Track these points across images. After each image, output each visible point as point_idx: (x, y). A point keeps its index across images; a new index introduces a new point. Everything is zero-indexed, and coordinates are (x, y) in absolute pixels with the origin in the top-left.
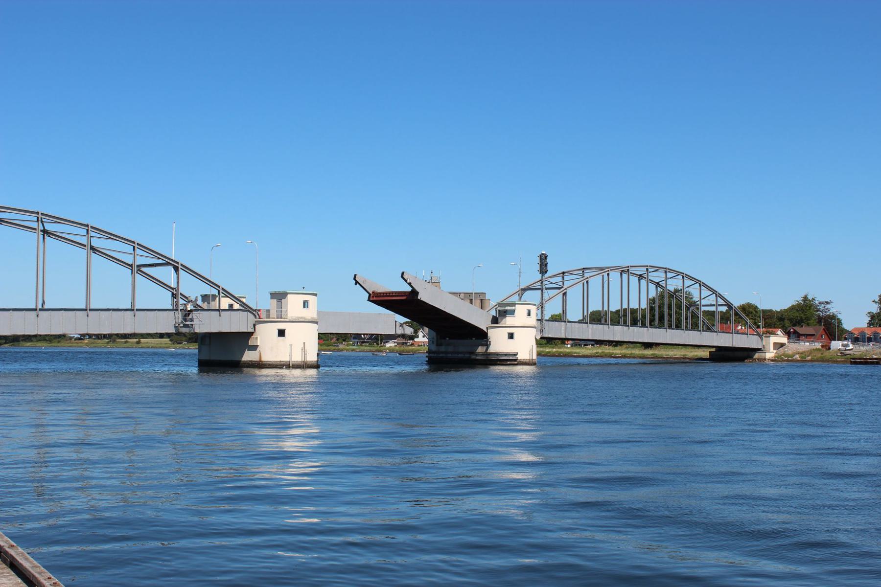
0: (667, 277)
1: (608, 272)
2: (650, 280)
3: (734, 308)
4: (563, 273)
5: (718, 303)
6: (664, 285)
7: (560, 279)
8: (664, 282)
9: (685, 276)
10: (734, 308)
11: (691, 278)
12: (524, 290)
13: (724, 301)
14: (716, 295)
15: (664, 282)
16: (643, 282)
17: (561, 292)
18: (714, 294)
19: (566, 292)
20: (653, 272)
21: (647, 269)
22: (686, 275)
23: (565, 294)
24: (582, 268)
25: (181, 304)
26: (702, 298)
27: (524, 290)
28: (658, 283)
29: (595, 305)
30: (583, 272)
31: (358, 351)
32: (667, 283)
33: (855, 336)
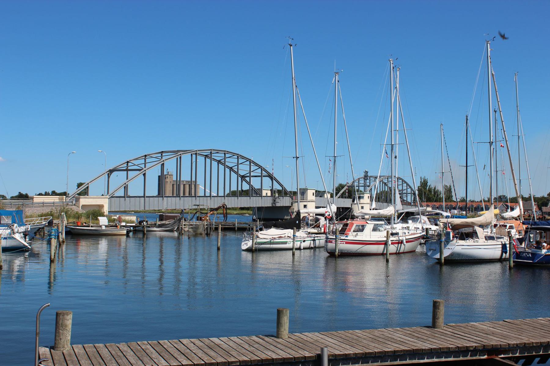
0: (226, 157)
1: (180, 156)
2: (213, 159)
3: (274, 178)
4: (146, 156)
5: (263, 175)
6: (236, 170)
7: (142, 161)
8: (223, 160)
9: (239, 156)
10: (274, 178)
11: (243, 158)
12: (111, 171)
13: (267, 173)
14: (262, 169)
15: (223, 160)
16: (208, 160)
17: (142, 173)
18: (260, 169)
19: (145, 173)
20: (215, 153)
21: (211, 152)
22: (240, 155)
23: (144, 175)
24: (161, 151)
25: (173, 195)
26: (252, 170)
27: (111, 171)
28: (231, 168)
29: (234, 188)
30: (162, 155)
31: (147, 212)
32: (239, 168)
33: (453, 206)
